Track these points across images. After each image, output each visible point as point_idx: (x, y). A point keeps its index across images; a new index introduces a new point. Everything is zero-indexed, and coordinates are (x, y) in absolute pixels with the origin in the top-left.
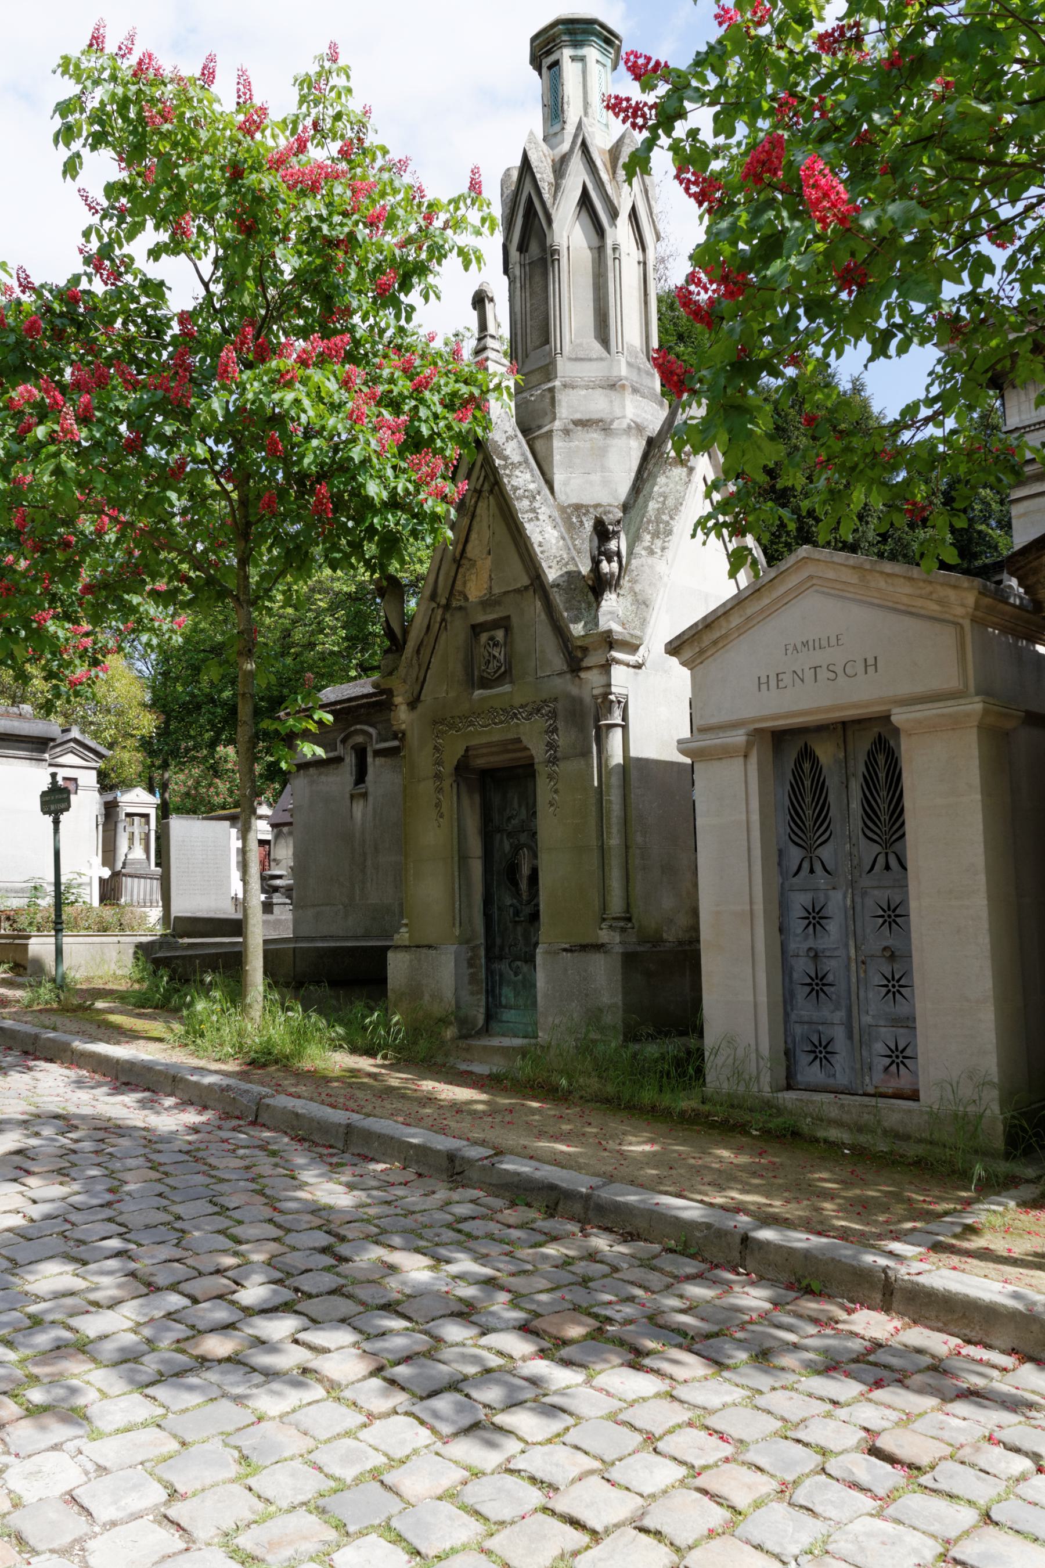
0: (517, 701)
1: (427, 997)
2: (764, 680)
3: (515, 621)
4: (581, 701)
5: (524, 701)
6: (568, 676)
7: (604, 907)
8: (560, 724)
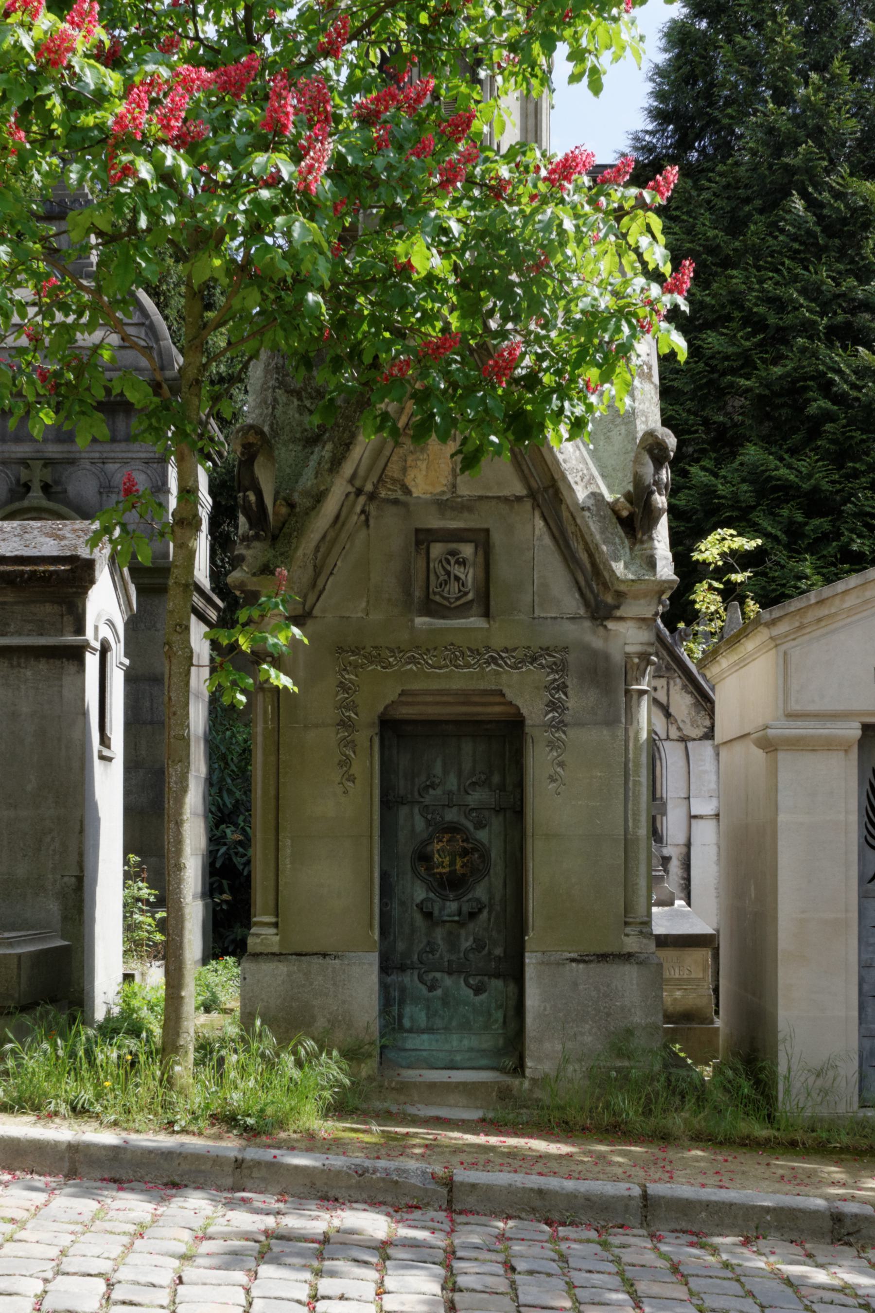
0: (498, 642)
3: (497, 538)
4: (607, 657)
5: (510, 645)
6: (587, 624)
8: (572, 682)
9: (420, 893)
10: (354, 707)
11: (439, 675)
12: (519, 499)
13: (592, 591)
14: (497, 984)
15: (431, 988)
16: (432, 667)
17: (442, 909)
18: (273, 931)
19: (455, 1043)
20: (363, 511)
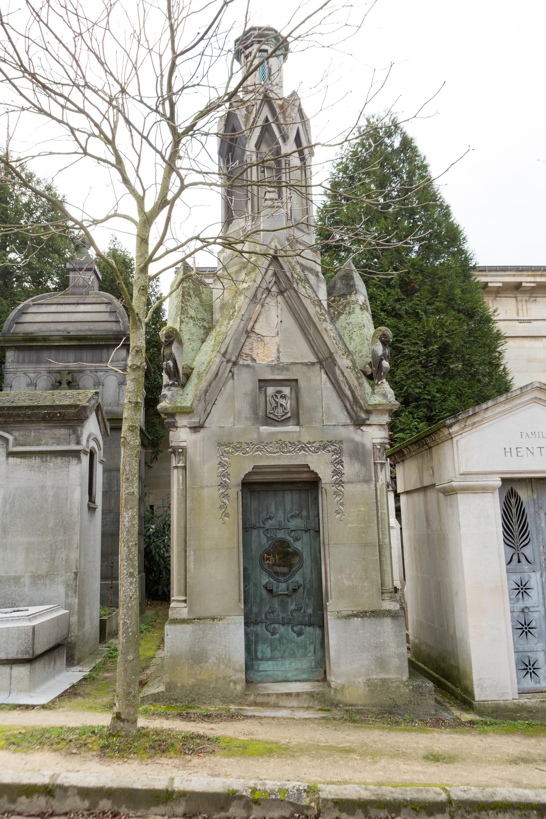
1: (212, 660)
2: (508, 450)
4: (363, 446)
6: (352, 428)
7: (382, 585)
9: (265, 579)
10: (227, 475)
11: (274, 457)
12: (313, 364)
14: (309, 630)
15: (273, 634)
16: (270, 453)
17: (278, 587)
18: (183, 605)
19: (287, 666)
20: (230, 371)
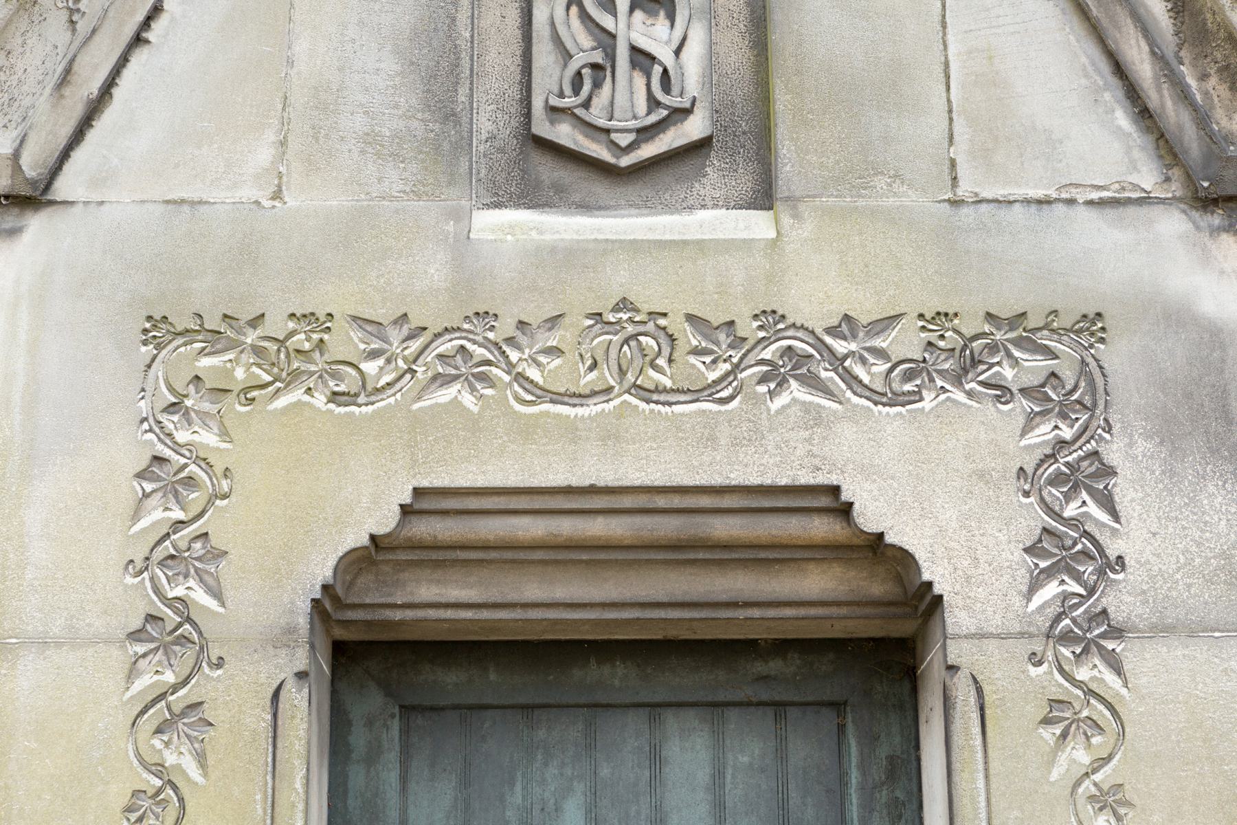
0: (814, 298)
5: (866, 310)
13: (1184, 95)
